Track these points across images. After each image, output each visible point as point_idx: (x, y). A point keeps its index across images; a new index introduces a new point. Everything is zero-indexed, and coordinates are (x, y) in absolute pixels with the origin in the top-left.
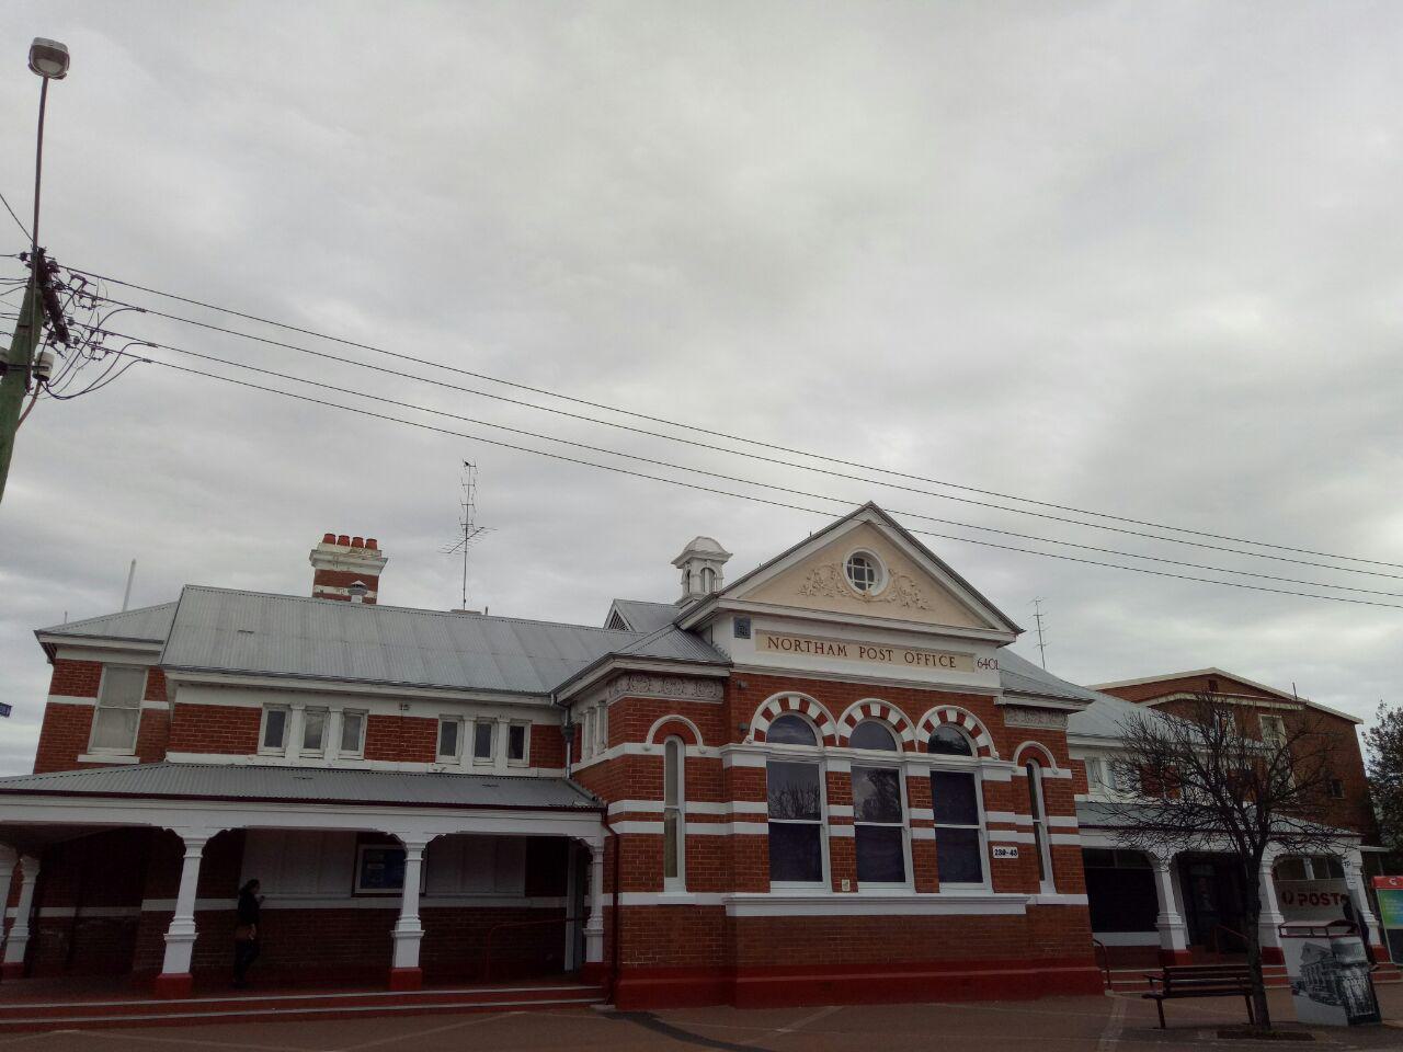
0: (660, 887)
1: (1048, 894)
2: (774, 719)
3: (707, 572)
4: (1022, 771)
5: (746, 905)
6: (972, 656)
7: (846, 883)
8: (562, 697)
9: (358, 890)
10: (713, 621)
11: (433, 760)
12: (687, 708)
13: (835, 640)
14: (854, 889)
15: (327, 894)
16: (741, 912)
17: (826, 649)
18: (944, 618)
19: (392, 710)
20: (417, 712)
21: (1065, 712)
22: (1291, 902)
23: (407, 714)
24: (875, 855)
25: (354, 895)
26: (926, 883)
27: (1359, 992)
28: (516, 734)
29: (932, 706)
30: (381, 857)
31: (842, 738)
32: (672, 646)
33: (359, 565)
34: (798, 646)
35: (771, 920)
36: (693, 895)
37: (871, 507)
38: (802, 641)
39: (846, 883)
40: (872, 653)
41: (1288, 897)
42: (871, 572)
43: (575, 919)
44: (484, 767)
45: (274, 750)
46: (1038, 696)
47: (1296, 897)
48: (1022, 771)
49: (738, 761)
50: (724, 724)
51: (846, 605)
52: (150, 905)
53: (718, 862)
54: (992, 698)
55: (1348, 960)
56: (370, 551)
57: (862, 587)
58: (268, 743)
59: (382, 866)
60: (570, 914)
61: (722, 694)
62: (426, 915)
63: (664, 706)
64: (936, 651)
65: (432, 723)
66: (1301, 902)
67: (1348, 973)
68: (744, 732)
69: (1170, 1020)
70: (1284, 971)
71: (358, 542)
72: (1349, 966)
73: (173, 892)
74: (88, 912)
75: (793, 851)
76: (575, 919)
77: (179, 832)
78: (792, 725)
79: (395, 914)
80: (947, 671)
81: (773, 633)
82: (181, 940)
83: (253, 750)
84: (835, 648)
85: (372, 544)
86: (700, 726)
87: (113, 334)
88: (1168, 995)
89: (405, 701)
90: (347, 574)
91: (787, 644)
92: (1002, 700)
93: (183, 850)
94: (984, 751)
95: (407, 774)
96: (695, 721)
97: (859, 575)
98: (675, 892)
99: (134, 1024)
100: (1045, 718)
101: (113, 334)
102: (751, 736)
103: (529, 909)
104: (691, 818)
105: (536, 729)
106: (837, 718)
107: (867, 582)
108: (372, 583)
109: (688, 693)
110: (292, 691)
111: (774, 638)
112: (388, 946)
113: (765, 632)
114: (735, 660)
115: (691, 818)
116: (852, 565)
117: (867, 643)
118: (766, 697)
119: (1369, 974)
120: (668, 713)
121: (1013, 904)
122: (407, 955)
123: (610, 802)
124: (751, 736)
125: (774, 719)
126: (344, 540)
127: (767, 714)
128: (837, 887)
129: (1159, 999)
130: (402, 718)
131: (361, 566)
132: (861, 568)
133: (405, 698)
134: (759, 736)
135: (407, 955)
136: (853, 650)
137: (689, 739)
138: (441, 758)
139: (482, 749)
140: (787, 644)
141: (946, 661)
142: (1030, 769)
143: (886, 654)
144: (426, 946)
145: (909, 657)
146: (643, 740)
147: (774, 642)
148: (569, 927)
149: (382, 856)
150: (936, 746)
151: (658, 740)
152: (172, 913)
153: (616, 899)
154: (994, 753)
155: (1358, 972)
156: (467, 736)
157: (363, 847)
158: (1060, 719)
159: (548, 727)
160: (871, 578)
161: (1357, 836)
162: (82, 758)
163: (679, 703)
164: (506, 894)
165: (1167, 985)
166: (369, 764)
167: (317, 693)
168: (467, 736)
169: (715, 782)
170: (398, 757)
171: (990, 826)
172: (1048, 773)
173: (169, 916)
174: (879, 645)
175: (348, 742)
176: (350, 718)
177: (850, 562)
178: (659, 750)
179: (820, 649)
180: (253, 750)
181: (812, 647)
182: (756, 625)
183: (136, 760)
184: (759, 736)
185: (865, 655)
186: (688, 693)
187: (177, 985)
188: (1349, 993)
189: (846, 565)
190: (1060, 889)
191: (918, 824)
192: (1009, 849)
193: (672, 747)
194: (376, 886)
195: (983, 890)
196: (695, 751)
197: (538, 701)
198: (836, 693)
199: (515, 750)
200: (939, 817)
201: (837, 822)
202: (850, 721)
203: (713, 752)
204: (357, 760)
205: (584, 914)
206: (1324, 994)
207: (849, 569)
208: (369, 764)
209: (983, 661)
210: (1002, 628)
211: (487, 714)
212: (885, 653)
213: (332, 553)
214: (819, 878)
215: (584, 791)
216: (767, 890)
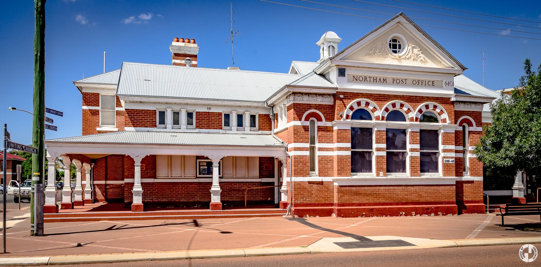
3: (331, 47)
4: (461, 129)
7: (381, 173)
8: (270, 103)
9: (198, 176)
10: (329, 70)
15: (189, 176)
19: (205, 110)
20: (213, 110)
21: (483, 103)
23: (210, 111)
25: (197, 177)
30: (205, 164)
36: (321, 178)
39: (381, 173)
42: (400, 45)
43: (278, 186)
45: (163, 126)
48: (461, 129)
52: (127, 180)
54: (450, 98)
59: (206, 167)
60: (276, 184)
61: (333, 101)
63: (310, 106)
65: (220, 114)
69: (505, 223)
73: (133, 177)
74: (109, 182)
76: (278, 186)
79: (211, 184)
86: (324, 113)
87: (7, 134)
88: (505, 215)
89: (209, 106)
92: (453, 99)
93: (134, 162)
94: (444, 121)
96: (321, 112)
97: (395, 46)
100: (473, 106)
101: (7, 134)
104: (320, 149)
105: (260, 115)
107: (398, 50)
109: (319, 101)
112: (209, 195)
115: (320, 149)
116: (392, 43)
120: (310, 109)
123: (288, 144)
125: (354, 110)
128: (378, 175)
129: (503, 215)
130: (208, 113)
133: (209, 105)
135: (137, 200)
142: (464, 127)
144: (144, 195)
145: (414, 82)
148: (276, 189)
151: (307, 119)
152: (134, 183)
153: (291, 179)
154: (448, 121)
157: (198, 160)
158: (481, 106)
159: (265, 115)
160: (400, 48)
161: (468, 202)
162: (98, 129)
163: (315, 105)
164: (253, 176)
172: (471, 129)
173: (132, 184)
177: (390, 41)
183: (117, 129)
189: (388, 42)
190: (472, 175)
192: (451, 160)
193: (313, 122)
194: (204, 174)
197: (260, 105)
200: (422, 147)
205: (280, 184)
207: (390, 44)
209: (447, 82)
214: (404, 170)
215: (279, 139)
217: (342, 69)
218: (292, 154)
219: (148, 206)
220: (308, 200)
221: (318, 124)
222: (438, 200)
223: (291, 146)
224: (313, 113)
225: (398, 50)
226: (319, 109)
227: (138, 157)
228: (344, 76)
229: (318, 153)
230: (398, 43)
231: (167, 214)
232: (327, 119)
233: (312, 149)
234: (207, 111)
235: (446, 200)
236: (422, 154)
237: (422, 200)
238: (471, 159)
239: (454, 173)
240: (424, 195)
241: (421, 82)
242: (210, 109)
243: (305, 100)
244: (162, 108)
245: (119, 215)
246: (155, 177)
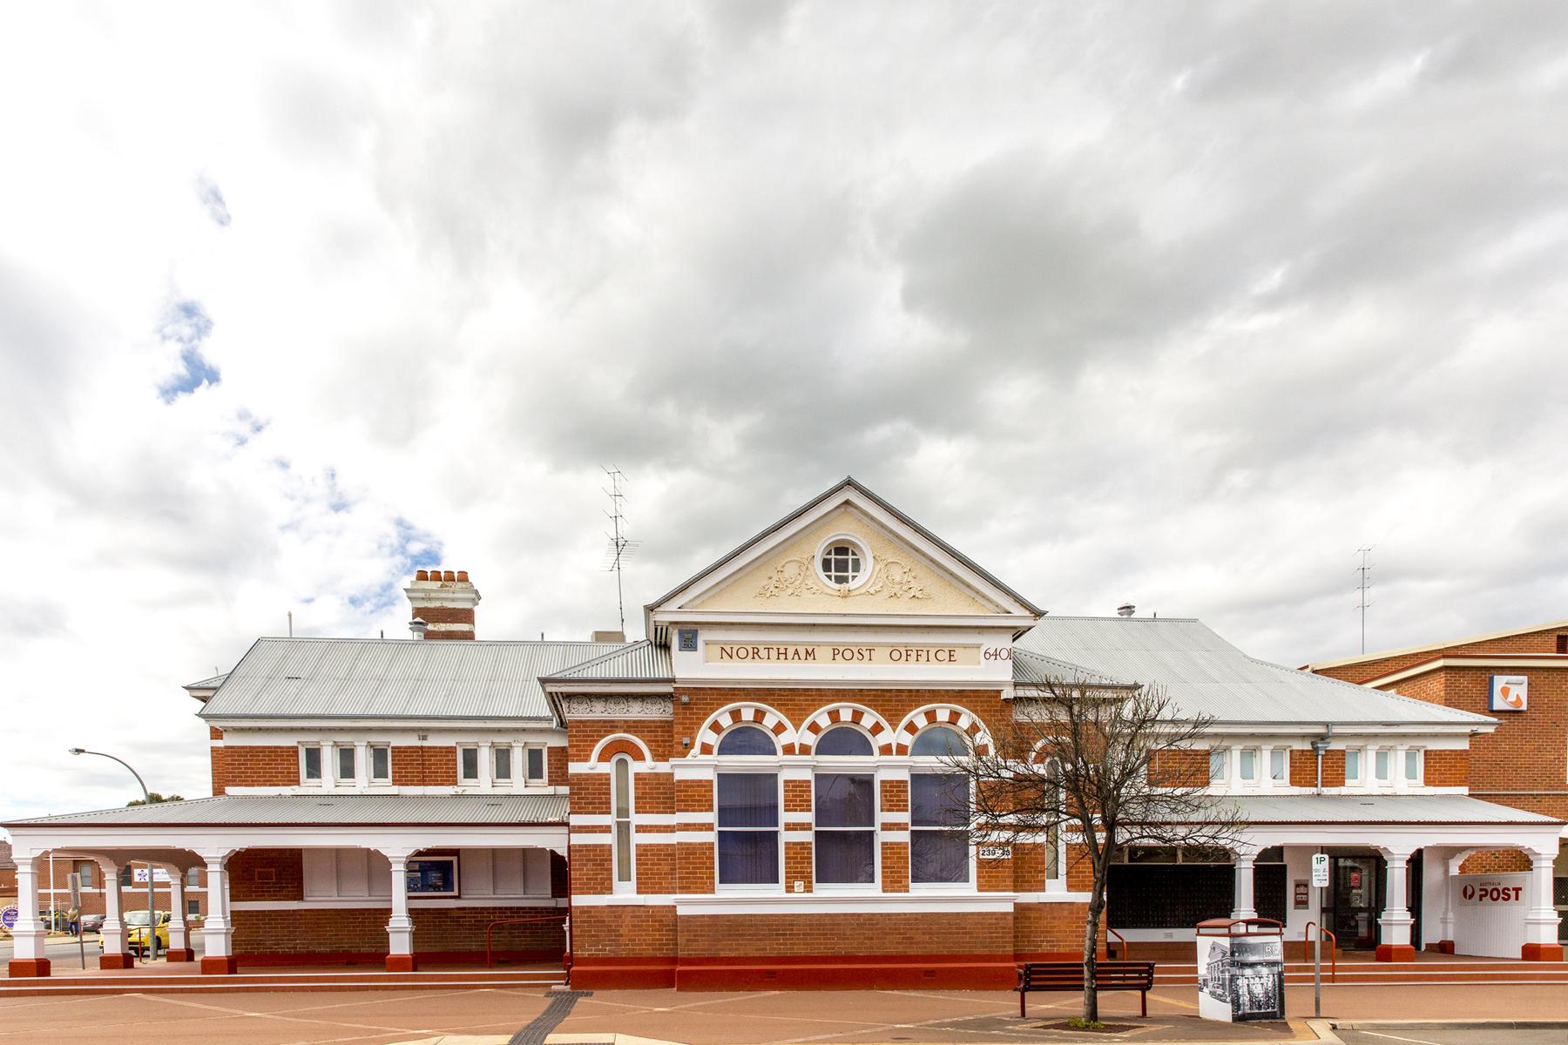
0: (607, 889)
1: (1056, 891)
2: (772, 735)
5: (690, 905)
6: (978, 646)
11: (455, 783)
12: (632, 726)
13: (802, 644)
14: (808, 889)
16: (681, 911)
17: (790, 653)
18: (948, 605)
19: (412, 741)
20: (434, 741)
22: (1471, 896)
23: (425, 744)
24: (842, 854)
26: (894, 882)
27: (1258, 991)
28: (534, 756)
29: (699, 725)
31: (899, 746)
32: (647, 666)
33: (454, 599)
34: (756, 653)
35: (715, 918)
36: (642, 896)
37: (849, 483)
38: (761, 648)
40: (848, 654)
41: (1469, 892)
44: (504, 788)
45: (315, 781)
46: (529, 719)
47: (1478, 893)
49: (680, 775)
50: (667, 741)
51: (818, 597)
53: (664, 868)
54: (999, 692)
55: (1252, 959)
56: (460, 585)
57: (840, 580)
58: (310, 775)
62: (414, 913)
63: (611, 726)
64: (933, 645)
65: (451, 751)
66: (1481, 897)
67: (1248, 972)
68: (689, 747)
70: (1195, 970)
71: (450, 576)
72: (1252, 965)
75: (749, 854)
77: (384, 852)
78: (743, 739)
79: (389, 911)
80: (946, 666)
81: (726, 643)
82: (24, 935)
83: (297, 782)
84: (803, 655)
85: (463, 577)
86: (648, 743)
89: (423, 733)
90: (444, 617)
91: (742, 653)
92: (1009, 693)
93: (390, 865)
95: (433, 797)
98: (625, 894)
99: (182, 991)
102: (697, 749)
103: (555, 909)
104: (641, 829)
106: (797, 727)
108: (467, 616)
109: (636, 712)
110: (321, 730)
111: (728, 649)
113: (715, 643)
114: (678, 675)
115: (641, 829)
117: (842, 644)
118: (713, 710)
119: (1280, 974)
120: (612, 732)
121: (1002, 902)
122: (400, 944)
124: (697, 749)
126: (436, 576)
127: (716, 727)
128: (790, 889)
131: (453, 600)
132: (840, 560)
133: (422, 729)
134: (706, 749)
135: (400, 944)
136: (823, 653)
137: (639, 756)
138: (808, 775)
139: (347, 771)
140: (742, 653)
141: (944, 655)
143: (866, 654)
144: (416, 937)
145: (896, 655)
146: (586, 759)
147: (727, 652)
149: (375, 865)
150: (925, 745)
151: (603, 757)
155: (1265, 971)
156: (486, 760)
165: (1027, 983)
166: (395, 790)
167: (342, 730)
168: (486, 760)
169: (663, 795)
170: (423, 782)
171: (709, 827)
174: (857, 644)
175: (380, 772)
176: (379, 754)
178: (607, 768)
179: (783, 654)
180: (297, 782)
181: (774, 653)
182: (703, 636)
184: (706, 749)
185: (839, 657)
186: (636, 712)
187: (399, 963)
188: (1243, 991)
191: (795, 828)
193: (622, 764)
195: (969, 889)
196: (648, 766)
198: (796, 700)
199: (534, 772)
201: (795, 828)
202: (814, 728)
203: (663, 767)
204: (386, 786)
206: (1220, 991)
208: (395, 790)
210: (1017, 610)
211: (502, 740)
212: (919, 654)
213: (423, 590)
214: (871, 879)
216: (712, 891)
217: (688, 632)
218: (637, 839)
219: (419, 960)
220: (608, 951)
221: (635, 767)
222: (966, 950)
223: (636, 819)
224: (621, 741)
225: (850, 574)
226: (635, 733)
227: (1248, 847)
228: (694, 648)
229: (637, 839)
230: (850, 557)
231: (1177, 971)
232: (660, 756)
233: (623, 829)
234: (418, 743)
235: (985, 951)
236: (915, 835)
237: (913, 951)
238: (1070, 847)
239: (1009, 882)
240: (918, 937)
241: (914, 654)
242: (424, 738)
243: (598, 712)
244: (469, 740)
245: (371, 979)
246: (299, 896)
